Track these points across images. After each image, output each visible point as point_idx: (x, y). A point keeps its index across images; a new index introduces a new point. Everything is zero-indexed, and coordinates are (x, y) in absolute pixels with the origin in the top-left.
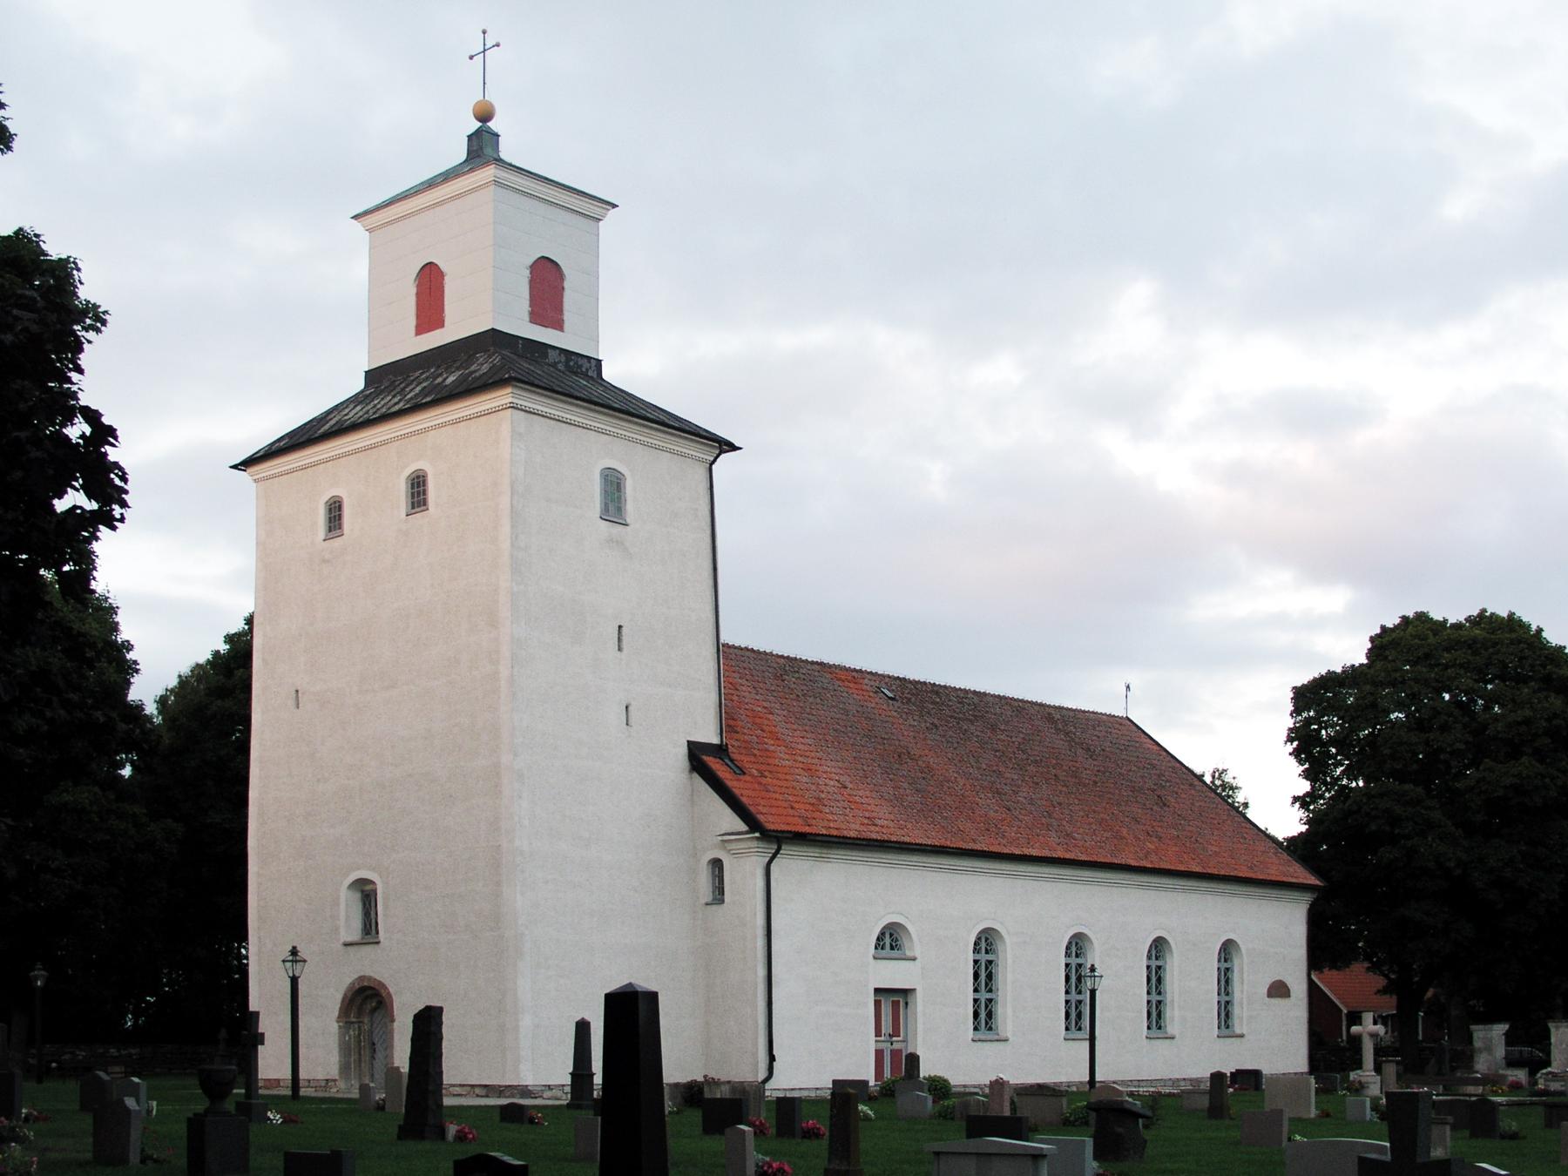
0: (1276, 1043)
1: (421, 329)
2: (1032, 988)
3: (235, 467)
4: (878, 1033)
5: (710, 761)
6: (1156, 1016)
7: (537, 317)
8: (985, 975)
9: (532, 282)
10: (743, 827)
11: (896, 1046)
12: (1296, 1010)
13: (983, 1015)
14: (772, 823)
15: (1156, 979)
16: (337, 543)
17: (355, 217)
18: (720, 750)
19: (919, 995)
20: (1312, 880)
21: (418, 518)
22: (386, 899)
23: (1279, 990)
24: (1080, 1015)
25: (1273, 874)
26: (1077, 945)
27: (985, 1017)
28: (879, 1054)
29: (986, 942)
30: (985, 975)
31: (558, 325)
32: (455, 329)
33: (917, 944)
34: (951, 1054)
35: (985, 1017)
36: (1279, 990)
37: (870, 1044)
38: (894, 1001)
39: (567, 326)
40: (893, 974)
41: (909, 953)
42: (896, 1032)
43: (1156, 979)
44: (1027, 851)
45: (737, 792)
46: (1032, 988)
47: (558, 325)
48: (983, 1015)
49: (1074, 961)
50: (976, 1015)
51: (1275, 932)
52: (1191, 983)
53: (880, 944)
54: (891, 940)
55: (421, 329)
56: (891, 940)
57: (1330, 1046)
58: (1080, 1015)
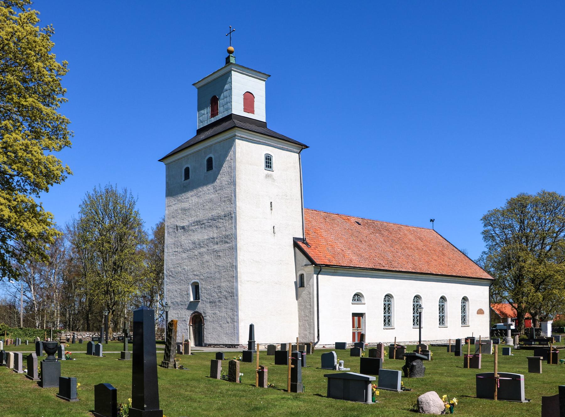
0: (480, 328)
1: (213, 115)
2: (403, 312)
3: (159, 161)
4: (353, 327)
5: (300, 244)
6: (442, 320)
7: (245, 110)
8: (387, 308)
9: (244, 99)
10: (309, 263)
11: (359, 331)
12: (486, 318)
13: (387, 321)
14: (318, 262)
15: (442, 309)
16: (187, 181)
17: (193, 85)
18: (303, 240)
19: (366, 315)
20: (486, 275)
21: (210, 172)
22: (307, 280)
23: (480, 312)
24: (418, 321)
25: (478, 275)
26: (417, 298)
27: (387, 321)
28: (354, 334)
29: (388, 297)
30: (387, 308)
31: (253, 112)
32: (220, 116)
33: (366, 300)
34: (376, 335)
35: (387, 321)
36: (480, 312)
37: (350, 330)
38: (358, 316)
39: (255, 112)
40: (358, 309)
41: (363, 302)
42: (359, 326)
43: (442, 309)
44: (401, 270)
45: (310, 255)
46: (403, 312)
47: (253, 112)
48: (387, 321)
49: (416, 304)
50: (385, 321)
51: (480, 295)
52: (453, 310)
53: (354, 299)
54: (358, 297)
55: (213, 115)
56: (358, 297)
57: (497, 333)
58: (418, 321)
